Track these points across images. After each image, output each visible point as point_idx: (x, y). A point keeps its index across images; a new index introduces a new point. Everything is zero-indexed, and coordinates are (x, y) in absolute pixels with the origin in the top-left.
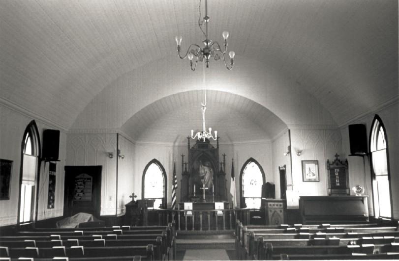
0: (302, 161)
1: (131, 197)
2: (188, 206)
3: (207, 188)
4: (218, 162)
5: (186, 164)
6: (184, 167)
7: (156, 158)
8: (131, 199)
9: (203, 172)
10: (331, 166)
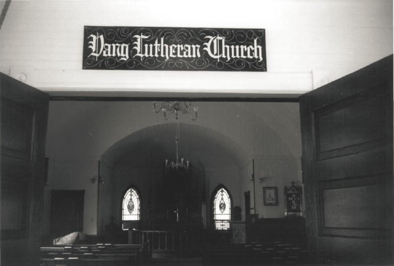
10: (288, 192)
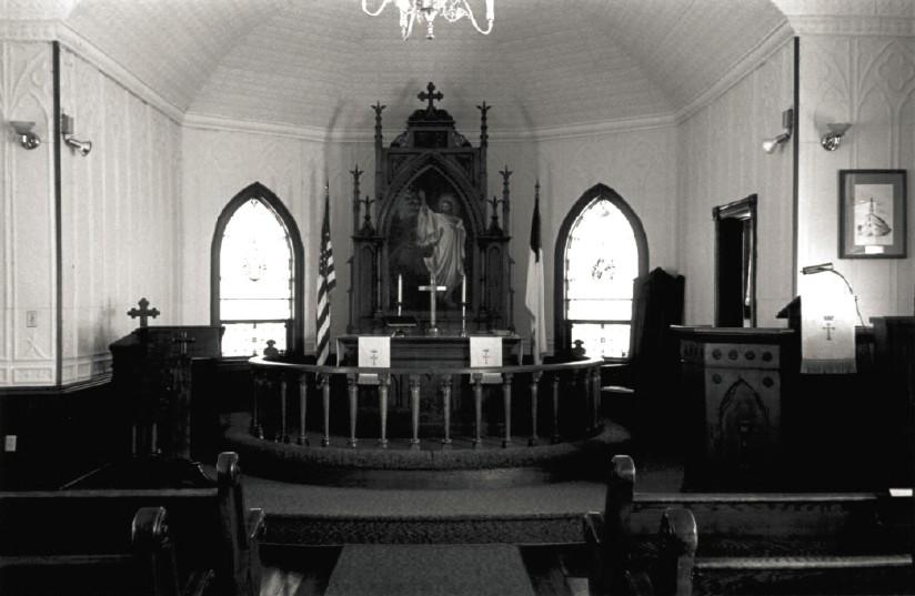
0: (842, 174)
1: (133, 313)
2: (375, 351)
3: (443, 288)
4: (483, 197)
5: (368, 203)
6: (362, 213)
7: (262, 182)
8: (136, 324)
9: (430, 231)
